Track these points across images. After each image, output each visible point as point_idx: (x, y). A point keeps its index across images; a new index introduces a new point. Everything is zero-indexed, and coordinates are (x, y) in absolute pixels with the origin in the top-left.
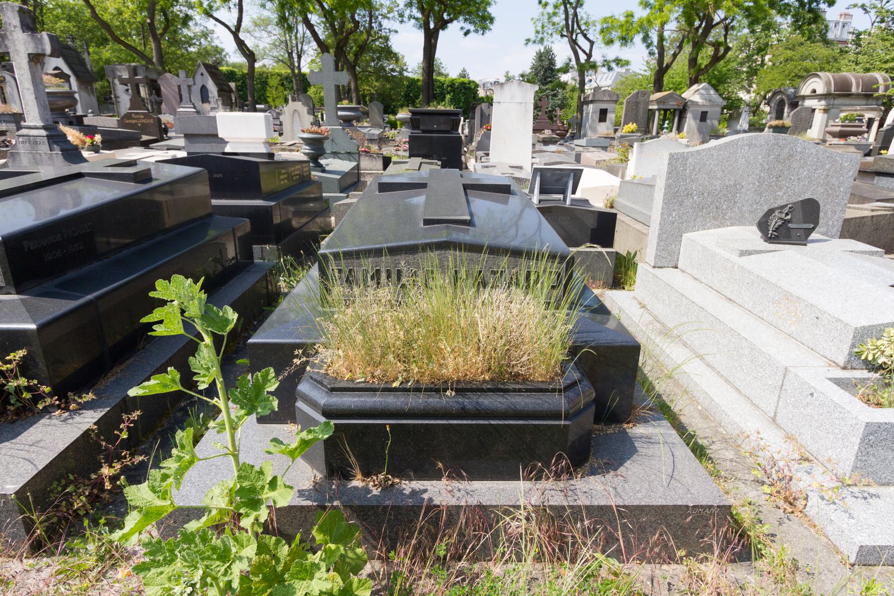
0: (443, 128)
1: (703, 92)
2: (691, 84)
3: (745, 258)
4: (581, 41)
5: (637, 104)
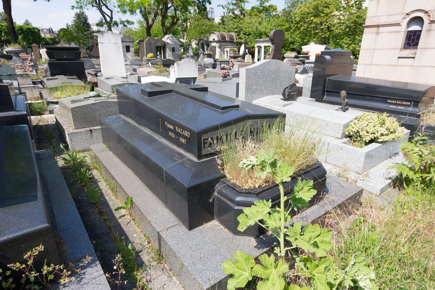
0: (70, 57)
1: (171, 38)
2: (165, 35)
3: (285, 107)
4: (104, 9)
5: (150, 44)
